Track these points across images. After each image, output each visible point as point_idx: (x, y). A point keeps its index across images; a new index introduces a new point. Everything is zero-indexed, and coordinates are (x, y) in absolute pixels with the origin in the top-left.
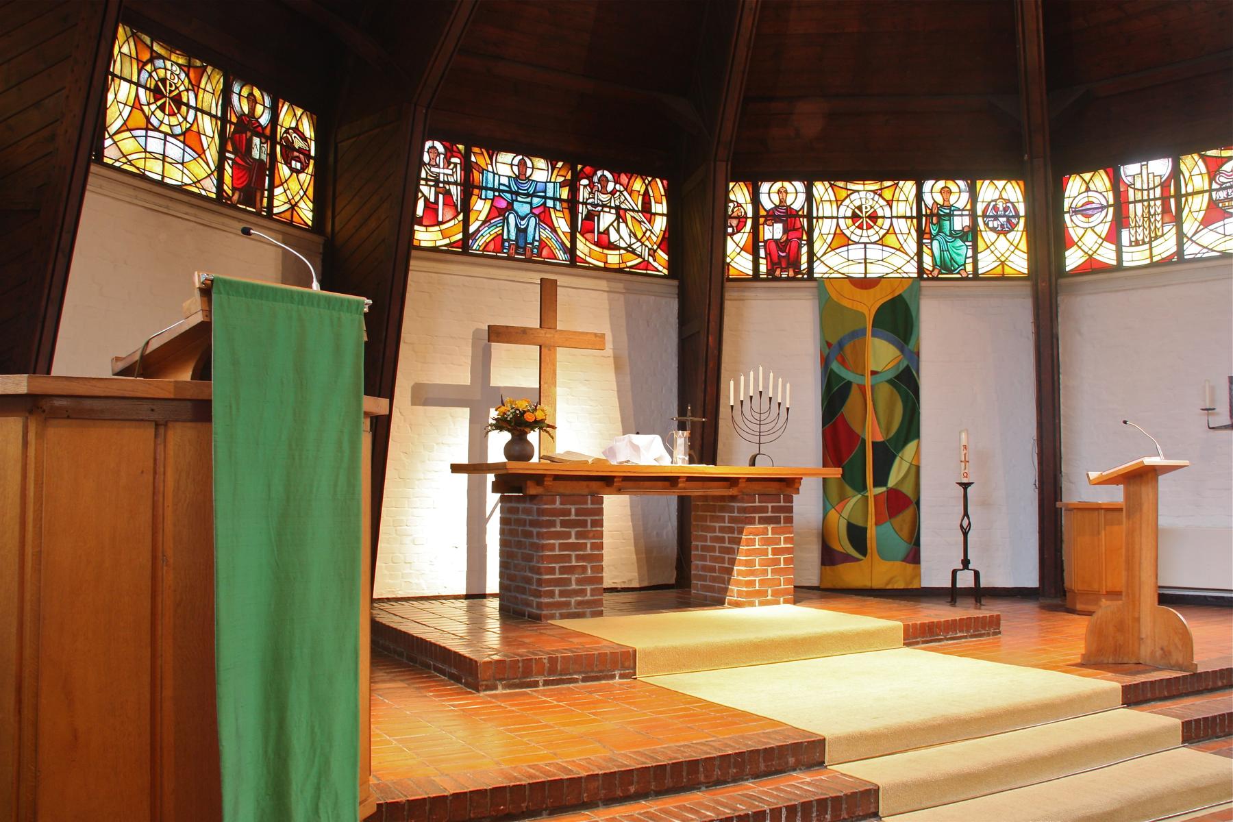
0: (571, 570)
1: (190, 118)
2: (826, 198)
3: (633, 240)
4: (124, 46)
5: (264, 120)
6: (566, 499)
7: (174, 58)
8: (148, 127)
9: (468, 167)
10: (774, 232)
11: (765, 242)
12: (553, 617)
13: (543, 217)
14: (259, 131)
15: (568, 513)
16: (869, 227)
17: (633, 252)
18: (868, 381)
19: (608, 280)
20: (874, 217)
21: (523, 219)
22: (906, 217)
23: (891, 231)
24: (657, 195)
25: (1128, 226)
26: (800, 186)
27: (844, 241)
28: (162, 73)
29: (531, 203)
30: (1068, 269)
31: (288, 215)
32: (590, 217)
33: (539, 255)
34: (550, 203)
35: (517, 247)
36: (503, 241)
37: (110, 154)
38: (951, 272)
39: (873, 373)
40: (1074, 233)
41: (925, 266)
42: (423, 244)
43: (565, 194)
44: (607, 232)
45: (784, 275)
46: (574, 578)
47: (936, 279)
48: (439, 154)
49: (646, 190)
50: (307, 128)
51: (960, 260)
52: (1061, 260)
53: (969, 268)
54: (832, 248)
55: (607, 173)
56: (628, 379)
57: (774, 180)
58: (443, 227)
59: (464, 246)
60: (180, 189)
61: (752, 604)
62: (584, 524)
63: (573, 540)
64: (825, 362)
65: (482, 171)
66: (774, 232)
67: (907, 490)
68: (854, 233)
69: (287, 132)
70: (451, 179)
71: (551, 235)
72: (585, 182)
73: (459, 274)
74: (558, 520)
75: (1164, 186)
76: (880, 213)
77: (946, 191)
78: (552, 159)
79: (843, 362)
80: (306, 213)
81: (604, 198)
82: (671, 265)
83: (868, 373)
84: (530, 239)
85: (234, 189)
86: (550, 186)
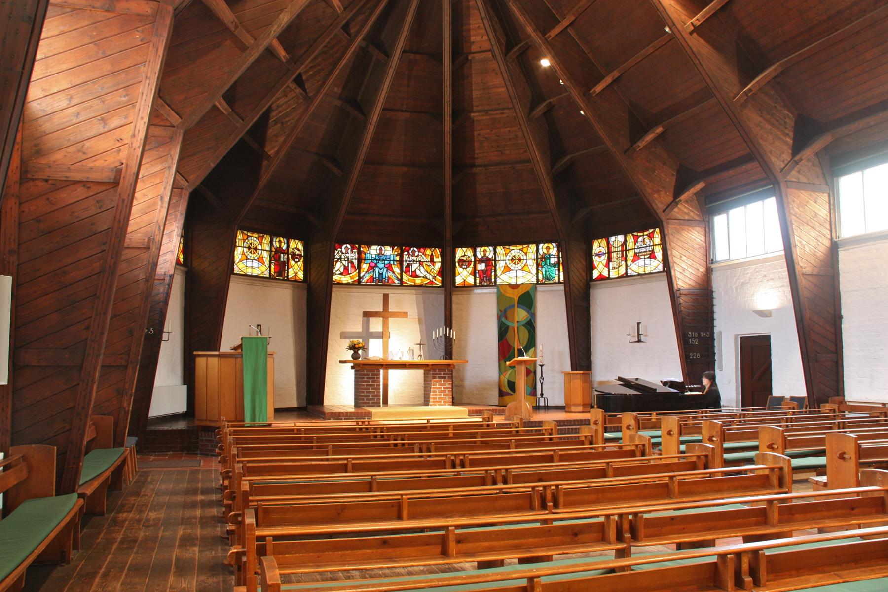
0: (370, 392)
1: (260, 253)
2: (501, 252)
3: (426, 273)
4: (240, 236)
5: (284, 247)
6: (368, 371)
7: (254, 236)
8: (247, 259)
9: (359, 252)
10: (482, 267)
11: (478, 271)
12: (364, 406)
13: (389, 268)
14: (283, 252)
15: (368, 375)
16: (518, 264)
17: (426, 278)
18: (515, 325)
19: (415, 289)
20: (520, 260)
21: (381, 269)
22: (532, 259)
23: (526, 265)
24: (437, 255)
25: (611, 262)
26: (491, 248)
27: (508, 269)
28: (250, 241)
29: (384, 263)
30: (594, 278)
31: (294, 278)
32: (408, 266)
33: (388, 282)
34: (392, 263)
35: (379, 280)
36: (374, 278)
37: (236, 270)
38: (550, 280)
39: (518, 322)
40: (596, 264)
41: (539, 278)
42: (344, 282)
43: (398, 258)
44: (415, 271)
45: (486, 284)
46: (371, 395)
47: (544, 284)
48: (348, 249)
49: (432, 254)
50: (300, 247)
51: (553, 275)
52: (591, 274)
53: (557, 279)
54: (503, 272)
55: (415, 249)
56: (424, 327)
57: (481, 246)
58: (351, 275)
59: (358, 283)
60: (257, 277)
61: (435, 405)
62: (374, 378)
63: (370, 383)
64: (499, 318)
65: (365, 253)
66: (482, 267)
67: (532, 370)
68: (511, 266)
69: (293, 249)
70: (353, 258)
71: (392, 274)
72: (406, 253)
73: (356, 292)
74: (365, 377)
75: (622, 246)
76: (522, 258)
77: (548, 248)
78: (392, 245)
79: (506, 318)
80: (301, 275)
81: (414, 258)
82: (443, 282)
83: (515, 322)
84: (384, 277)
85: (275, 273)
86: (392, 256)
